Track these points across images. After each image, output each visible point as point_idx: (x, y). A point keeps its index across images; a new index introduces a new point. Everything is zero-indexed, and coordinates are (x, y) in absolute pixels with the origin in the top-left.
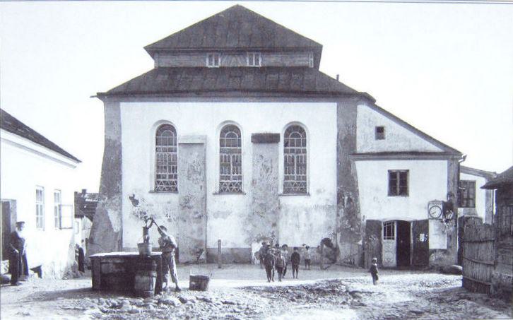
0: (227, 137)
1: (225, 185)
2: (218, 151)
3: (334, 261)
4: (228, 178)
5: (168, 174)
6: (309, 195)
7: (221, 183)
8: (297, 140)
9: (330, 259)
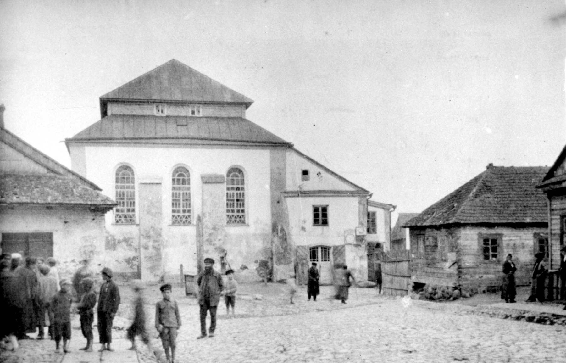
0: (232, 177)
1: (120, 217)
2: (171, 188)
3: (270, 280)
4: (179, 211)
5: (125, 208)
6: (248, 225)
7: (173, 216)
8: (237, 179)
9: (84, 292)
